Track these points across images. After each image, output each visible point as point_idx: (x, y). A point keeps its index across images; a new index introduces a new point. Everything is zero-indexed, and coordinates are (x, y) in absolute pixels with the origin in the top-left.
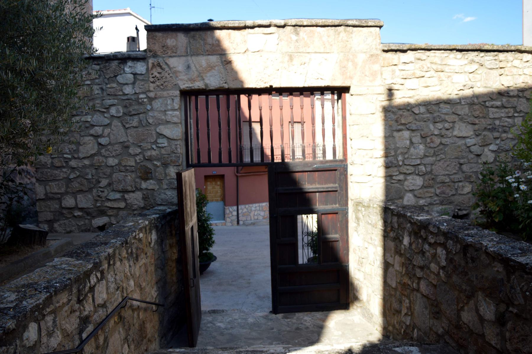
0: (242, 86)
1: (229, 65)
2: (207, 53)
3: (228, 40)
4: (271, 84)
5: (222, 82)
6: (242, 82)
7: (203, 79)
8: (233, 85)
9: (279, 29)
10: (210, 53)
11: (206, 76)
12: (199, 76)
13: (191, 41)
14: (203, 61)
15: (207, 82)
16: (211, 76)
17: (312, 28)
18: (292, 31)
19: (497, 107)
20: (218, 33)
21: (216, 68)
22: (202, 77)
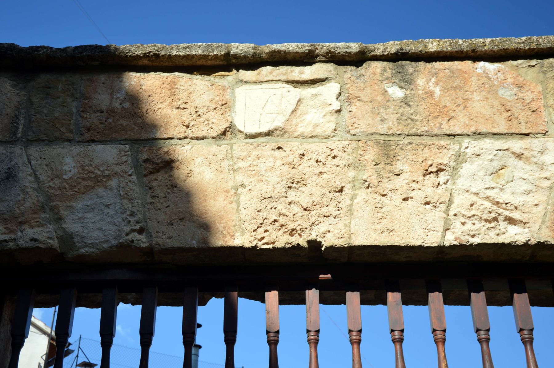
0: (205, 240)
1: (161, 176)
2: (87, 136)
3: (171, 100)
4: (313, 237)
5: (127, 229)
6: (205, 227)
7: (59, 219)
8: (170, 237)
9: (342, 69)
10: (97, 137)
11: (71, 208)
12: (42, 209)
13: (35, 100)
14: (68, 160)
15: (72, 225)
16: (90, 209)
17: (457, 64)
18: (388, 74)
19: (511, 221)
20: (135, 80)
21: (114, 183)
22: (54, 210)
